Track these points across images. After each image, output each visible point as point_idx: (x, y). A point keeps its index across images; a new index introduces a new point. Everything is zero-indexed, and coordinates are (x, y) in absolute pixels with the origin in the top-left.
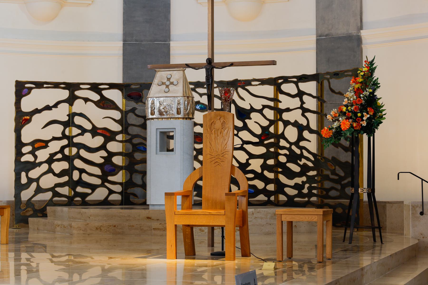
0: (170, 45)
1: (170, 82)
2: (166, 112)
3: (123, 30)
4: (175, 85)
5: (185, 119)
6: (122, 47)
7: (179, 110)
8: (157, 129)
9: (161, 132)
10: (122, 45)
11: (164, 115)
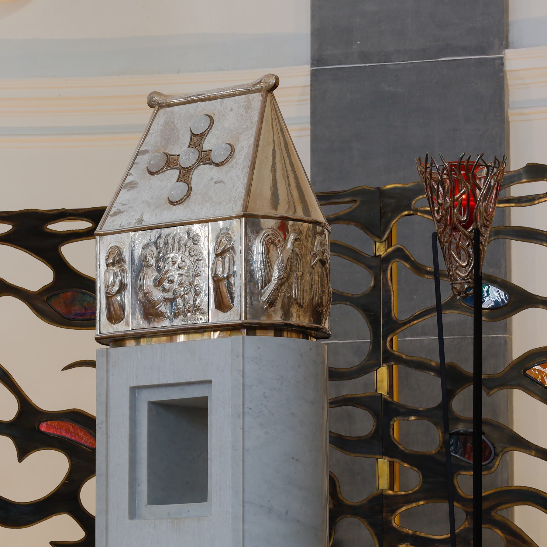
0: (502, 64)
1: (200, 152)
2: (171, 301)
3: (313, 17)
4: (217, 165)
5: (244, 331)
6: (308, 90)
7: (224, 286)
8: (135, 390)
9: (155, 405)
10: (307, 80)
11: (160, 315)
